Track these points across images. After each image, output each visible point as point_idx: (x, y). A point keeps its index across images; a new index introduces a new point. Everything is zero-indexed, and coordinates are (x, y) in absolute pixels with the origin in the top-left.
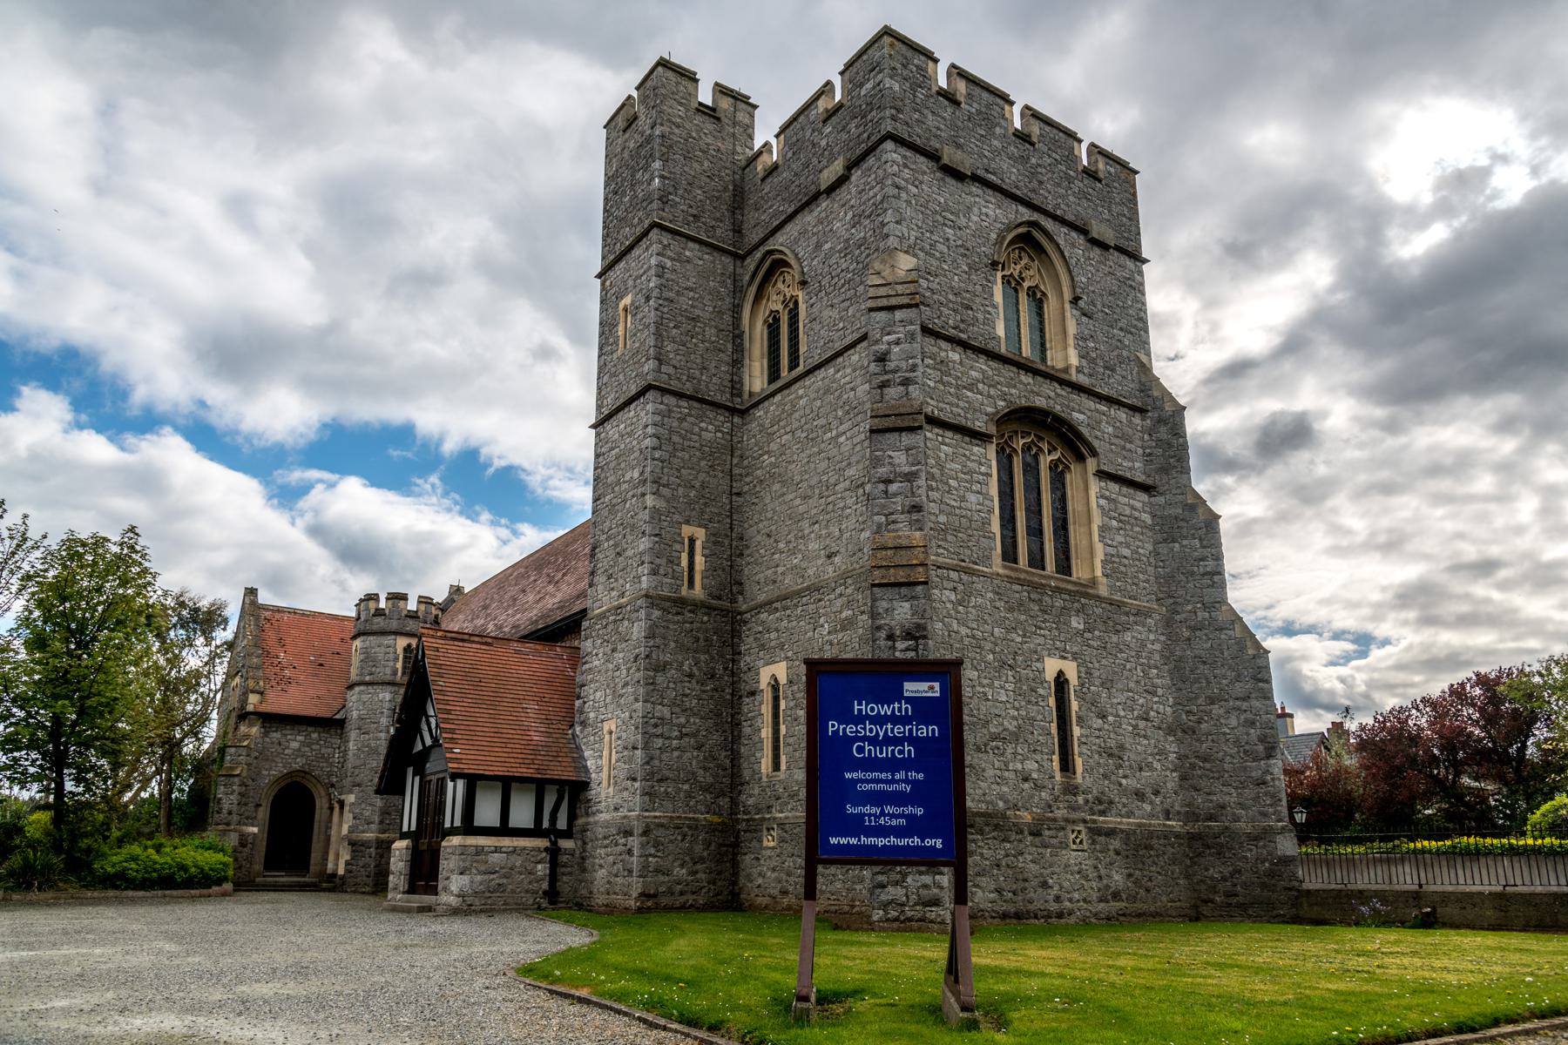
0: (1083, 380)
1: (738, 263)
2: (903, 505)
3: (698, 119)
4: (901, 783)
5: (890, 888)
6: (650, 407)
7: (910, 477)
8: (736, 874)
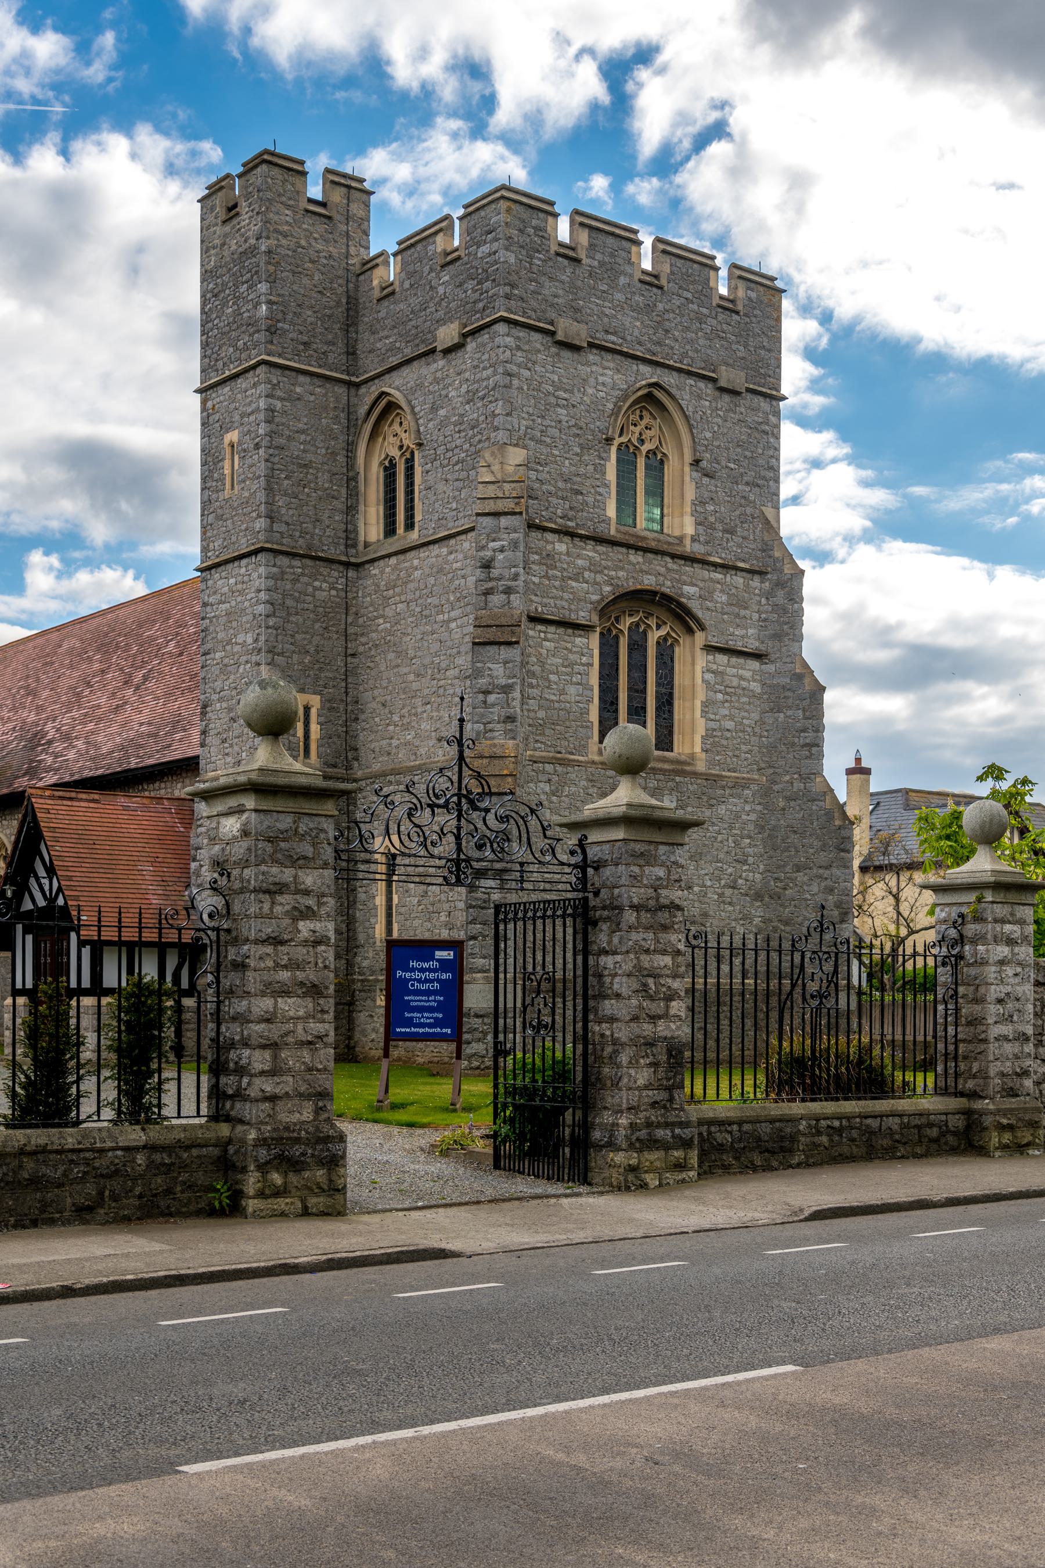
0: (699, 549)
1: (353, 391)
2: (499, 716)
3: (307, 223)
4: (433, 1001)
5: (474, 1044)
6: (262, 569)
7: (506, 689)
8: (351, 1029)
